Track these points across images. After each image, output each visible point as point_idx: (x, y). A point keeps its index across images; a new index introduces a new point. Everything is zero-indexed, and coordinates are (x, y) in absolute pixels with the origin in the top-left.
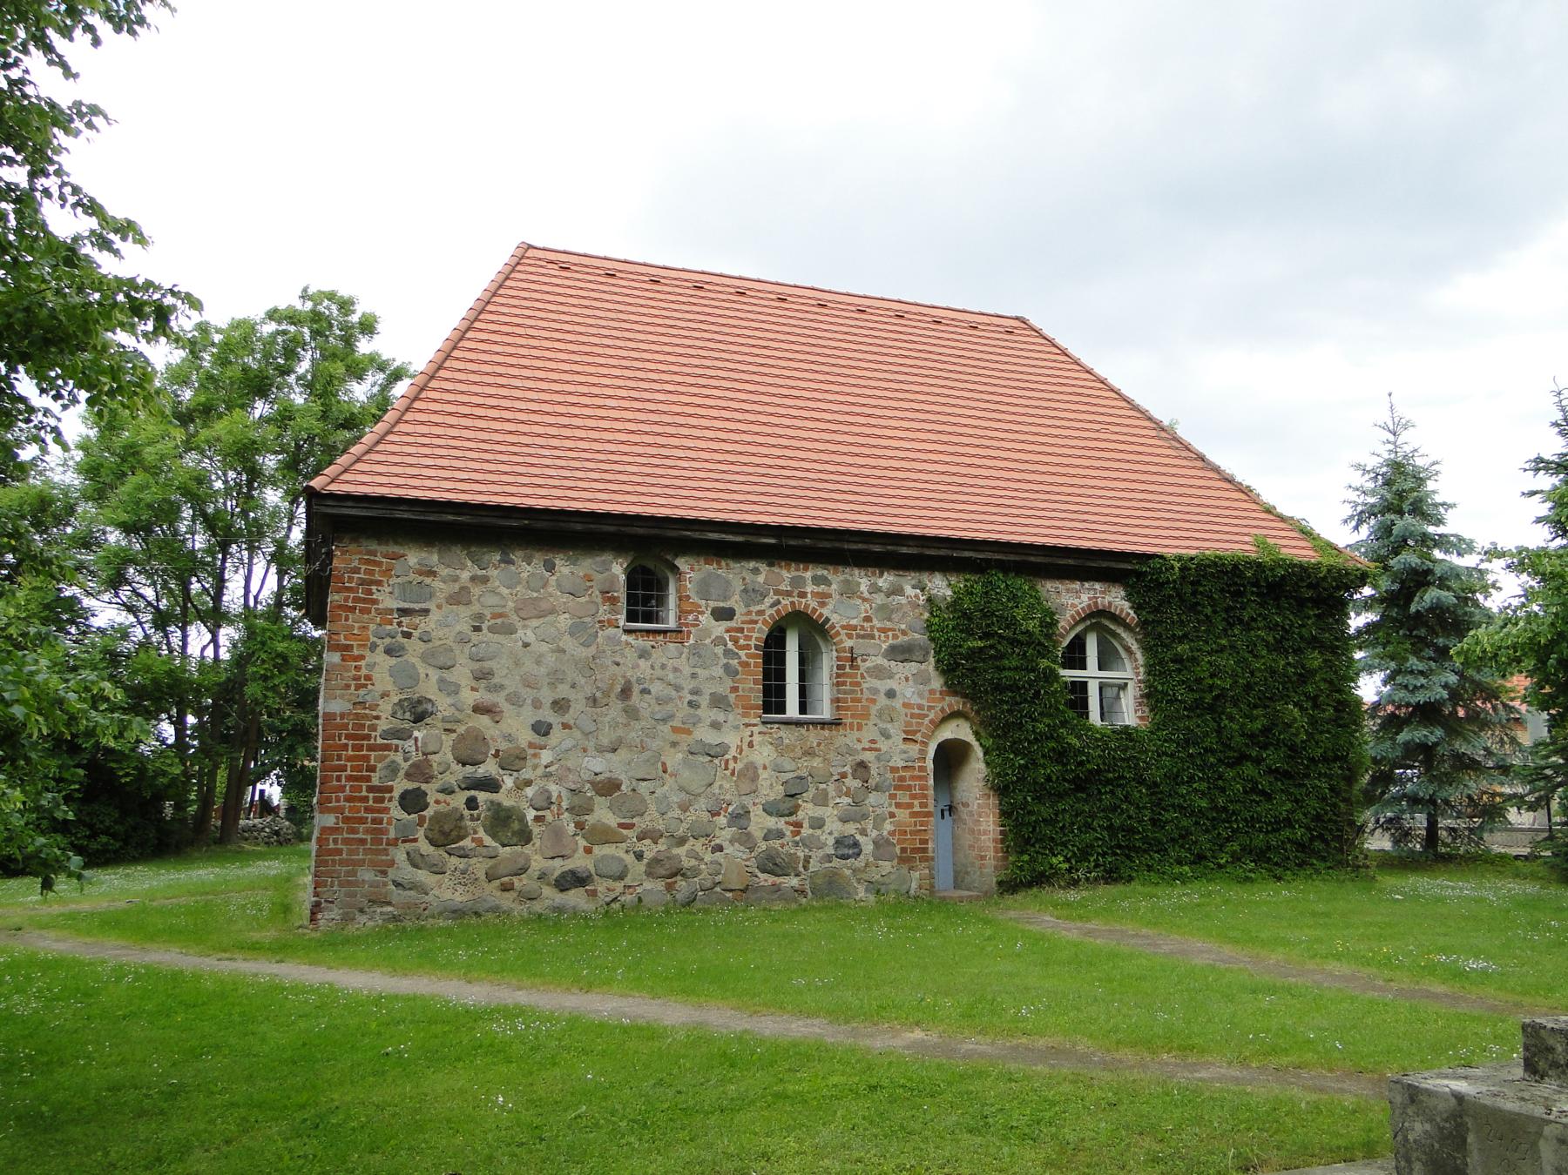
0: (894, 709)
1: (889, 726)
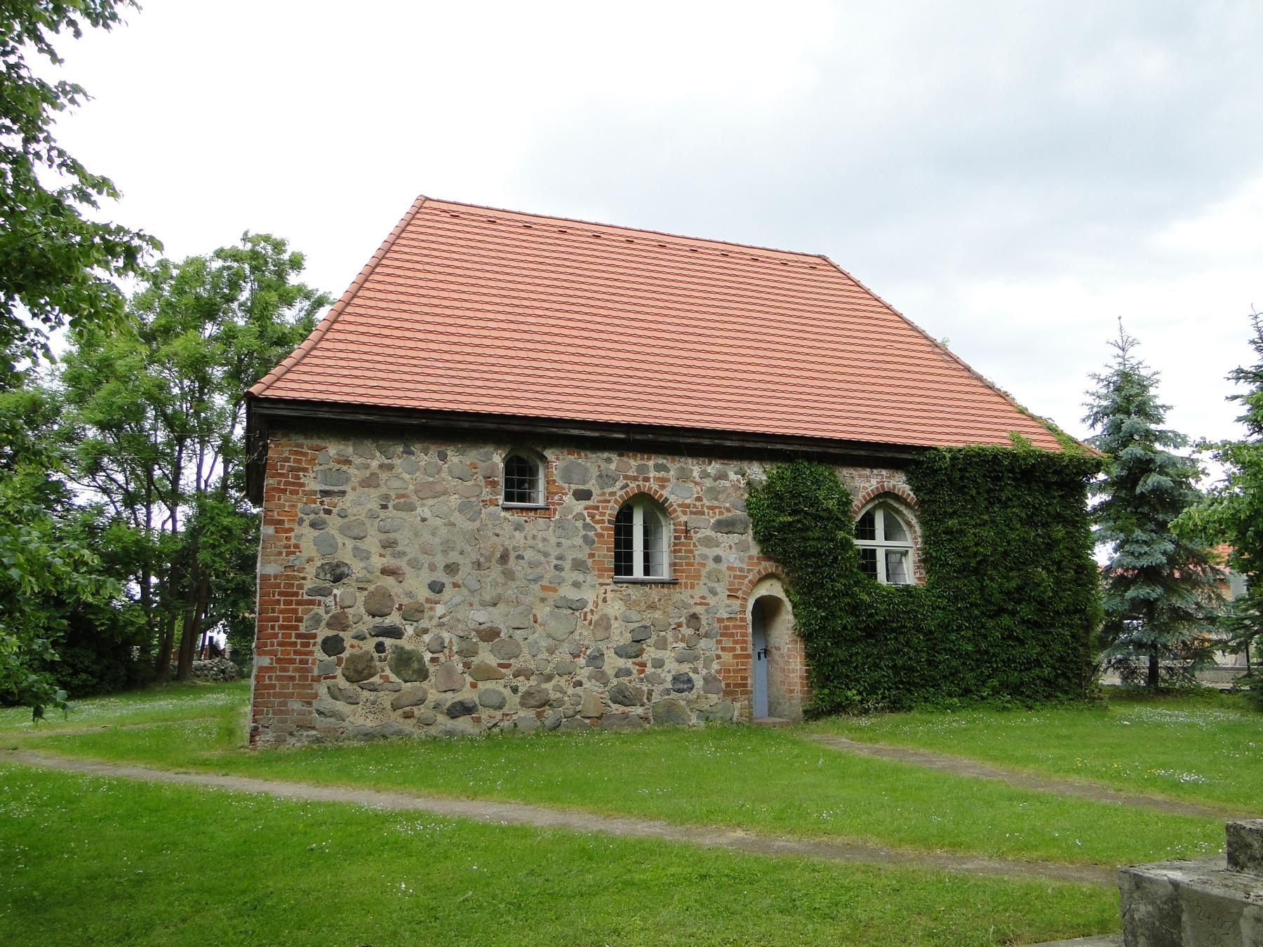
0: (720, 571)
1: (716, 585)
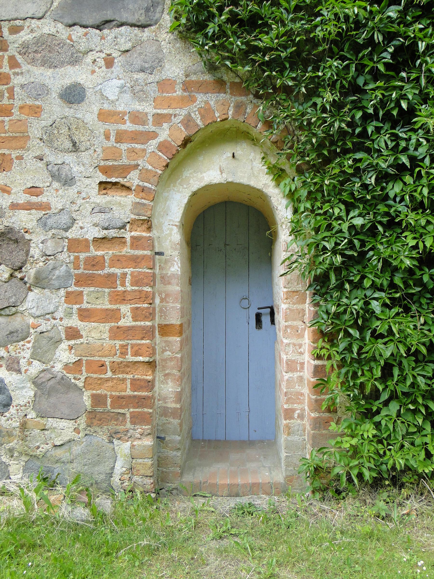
0: (82, 125)
1: (70, 158)
